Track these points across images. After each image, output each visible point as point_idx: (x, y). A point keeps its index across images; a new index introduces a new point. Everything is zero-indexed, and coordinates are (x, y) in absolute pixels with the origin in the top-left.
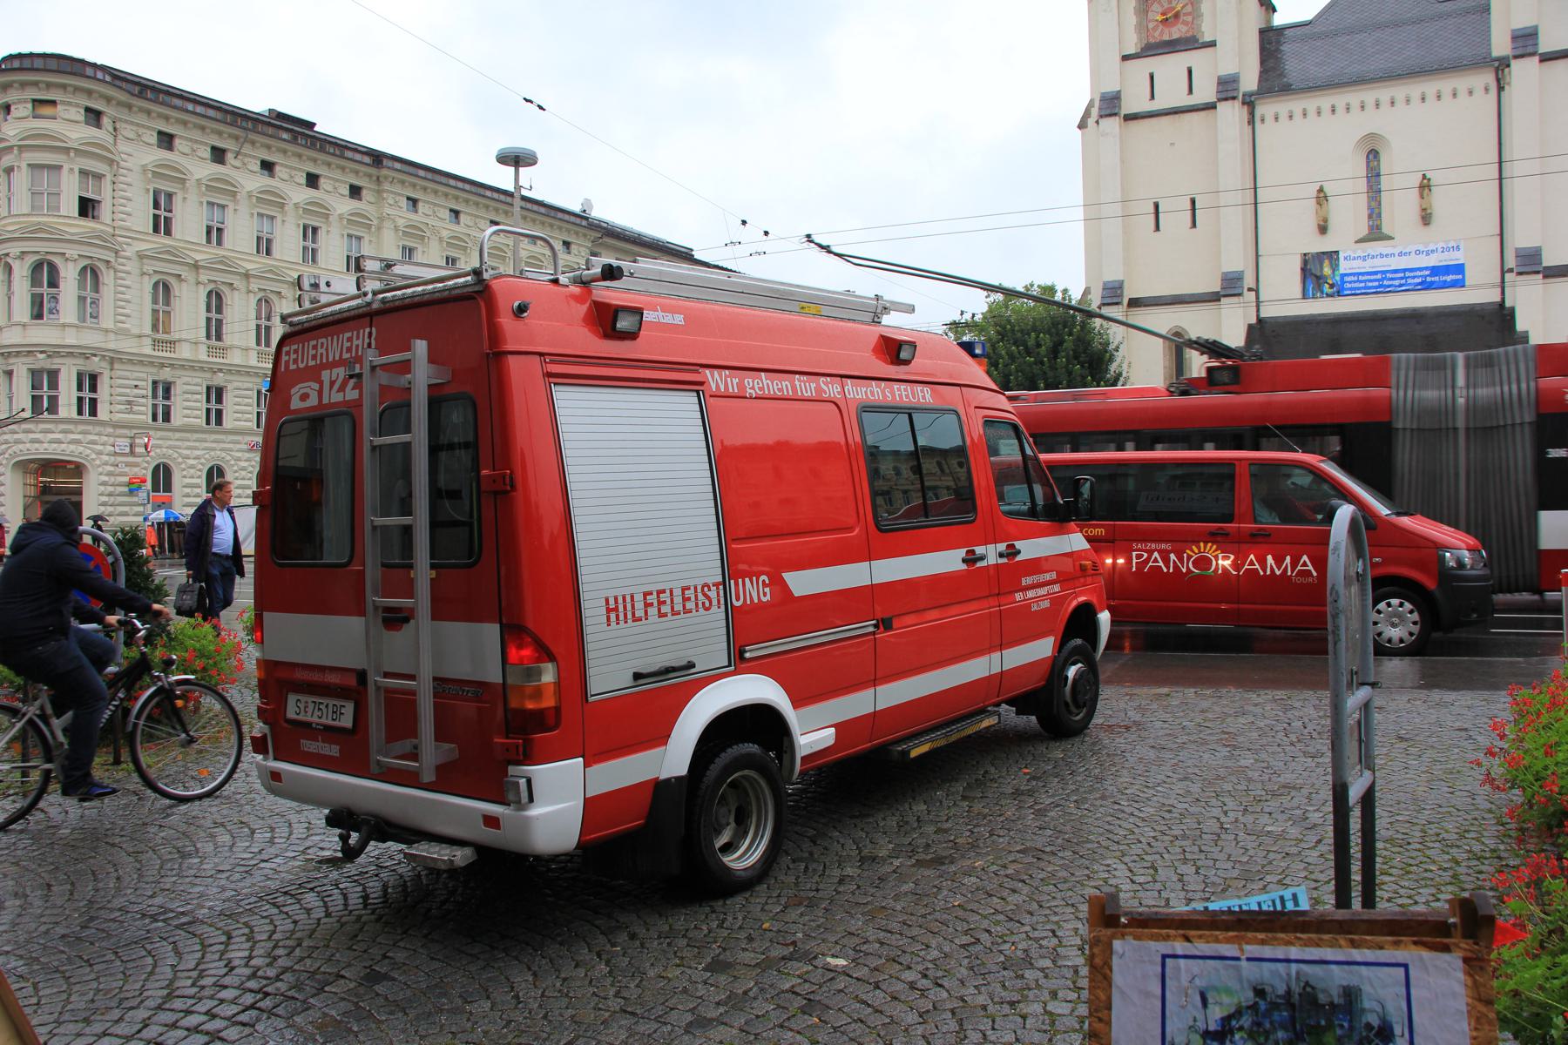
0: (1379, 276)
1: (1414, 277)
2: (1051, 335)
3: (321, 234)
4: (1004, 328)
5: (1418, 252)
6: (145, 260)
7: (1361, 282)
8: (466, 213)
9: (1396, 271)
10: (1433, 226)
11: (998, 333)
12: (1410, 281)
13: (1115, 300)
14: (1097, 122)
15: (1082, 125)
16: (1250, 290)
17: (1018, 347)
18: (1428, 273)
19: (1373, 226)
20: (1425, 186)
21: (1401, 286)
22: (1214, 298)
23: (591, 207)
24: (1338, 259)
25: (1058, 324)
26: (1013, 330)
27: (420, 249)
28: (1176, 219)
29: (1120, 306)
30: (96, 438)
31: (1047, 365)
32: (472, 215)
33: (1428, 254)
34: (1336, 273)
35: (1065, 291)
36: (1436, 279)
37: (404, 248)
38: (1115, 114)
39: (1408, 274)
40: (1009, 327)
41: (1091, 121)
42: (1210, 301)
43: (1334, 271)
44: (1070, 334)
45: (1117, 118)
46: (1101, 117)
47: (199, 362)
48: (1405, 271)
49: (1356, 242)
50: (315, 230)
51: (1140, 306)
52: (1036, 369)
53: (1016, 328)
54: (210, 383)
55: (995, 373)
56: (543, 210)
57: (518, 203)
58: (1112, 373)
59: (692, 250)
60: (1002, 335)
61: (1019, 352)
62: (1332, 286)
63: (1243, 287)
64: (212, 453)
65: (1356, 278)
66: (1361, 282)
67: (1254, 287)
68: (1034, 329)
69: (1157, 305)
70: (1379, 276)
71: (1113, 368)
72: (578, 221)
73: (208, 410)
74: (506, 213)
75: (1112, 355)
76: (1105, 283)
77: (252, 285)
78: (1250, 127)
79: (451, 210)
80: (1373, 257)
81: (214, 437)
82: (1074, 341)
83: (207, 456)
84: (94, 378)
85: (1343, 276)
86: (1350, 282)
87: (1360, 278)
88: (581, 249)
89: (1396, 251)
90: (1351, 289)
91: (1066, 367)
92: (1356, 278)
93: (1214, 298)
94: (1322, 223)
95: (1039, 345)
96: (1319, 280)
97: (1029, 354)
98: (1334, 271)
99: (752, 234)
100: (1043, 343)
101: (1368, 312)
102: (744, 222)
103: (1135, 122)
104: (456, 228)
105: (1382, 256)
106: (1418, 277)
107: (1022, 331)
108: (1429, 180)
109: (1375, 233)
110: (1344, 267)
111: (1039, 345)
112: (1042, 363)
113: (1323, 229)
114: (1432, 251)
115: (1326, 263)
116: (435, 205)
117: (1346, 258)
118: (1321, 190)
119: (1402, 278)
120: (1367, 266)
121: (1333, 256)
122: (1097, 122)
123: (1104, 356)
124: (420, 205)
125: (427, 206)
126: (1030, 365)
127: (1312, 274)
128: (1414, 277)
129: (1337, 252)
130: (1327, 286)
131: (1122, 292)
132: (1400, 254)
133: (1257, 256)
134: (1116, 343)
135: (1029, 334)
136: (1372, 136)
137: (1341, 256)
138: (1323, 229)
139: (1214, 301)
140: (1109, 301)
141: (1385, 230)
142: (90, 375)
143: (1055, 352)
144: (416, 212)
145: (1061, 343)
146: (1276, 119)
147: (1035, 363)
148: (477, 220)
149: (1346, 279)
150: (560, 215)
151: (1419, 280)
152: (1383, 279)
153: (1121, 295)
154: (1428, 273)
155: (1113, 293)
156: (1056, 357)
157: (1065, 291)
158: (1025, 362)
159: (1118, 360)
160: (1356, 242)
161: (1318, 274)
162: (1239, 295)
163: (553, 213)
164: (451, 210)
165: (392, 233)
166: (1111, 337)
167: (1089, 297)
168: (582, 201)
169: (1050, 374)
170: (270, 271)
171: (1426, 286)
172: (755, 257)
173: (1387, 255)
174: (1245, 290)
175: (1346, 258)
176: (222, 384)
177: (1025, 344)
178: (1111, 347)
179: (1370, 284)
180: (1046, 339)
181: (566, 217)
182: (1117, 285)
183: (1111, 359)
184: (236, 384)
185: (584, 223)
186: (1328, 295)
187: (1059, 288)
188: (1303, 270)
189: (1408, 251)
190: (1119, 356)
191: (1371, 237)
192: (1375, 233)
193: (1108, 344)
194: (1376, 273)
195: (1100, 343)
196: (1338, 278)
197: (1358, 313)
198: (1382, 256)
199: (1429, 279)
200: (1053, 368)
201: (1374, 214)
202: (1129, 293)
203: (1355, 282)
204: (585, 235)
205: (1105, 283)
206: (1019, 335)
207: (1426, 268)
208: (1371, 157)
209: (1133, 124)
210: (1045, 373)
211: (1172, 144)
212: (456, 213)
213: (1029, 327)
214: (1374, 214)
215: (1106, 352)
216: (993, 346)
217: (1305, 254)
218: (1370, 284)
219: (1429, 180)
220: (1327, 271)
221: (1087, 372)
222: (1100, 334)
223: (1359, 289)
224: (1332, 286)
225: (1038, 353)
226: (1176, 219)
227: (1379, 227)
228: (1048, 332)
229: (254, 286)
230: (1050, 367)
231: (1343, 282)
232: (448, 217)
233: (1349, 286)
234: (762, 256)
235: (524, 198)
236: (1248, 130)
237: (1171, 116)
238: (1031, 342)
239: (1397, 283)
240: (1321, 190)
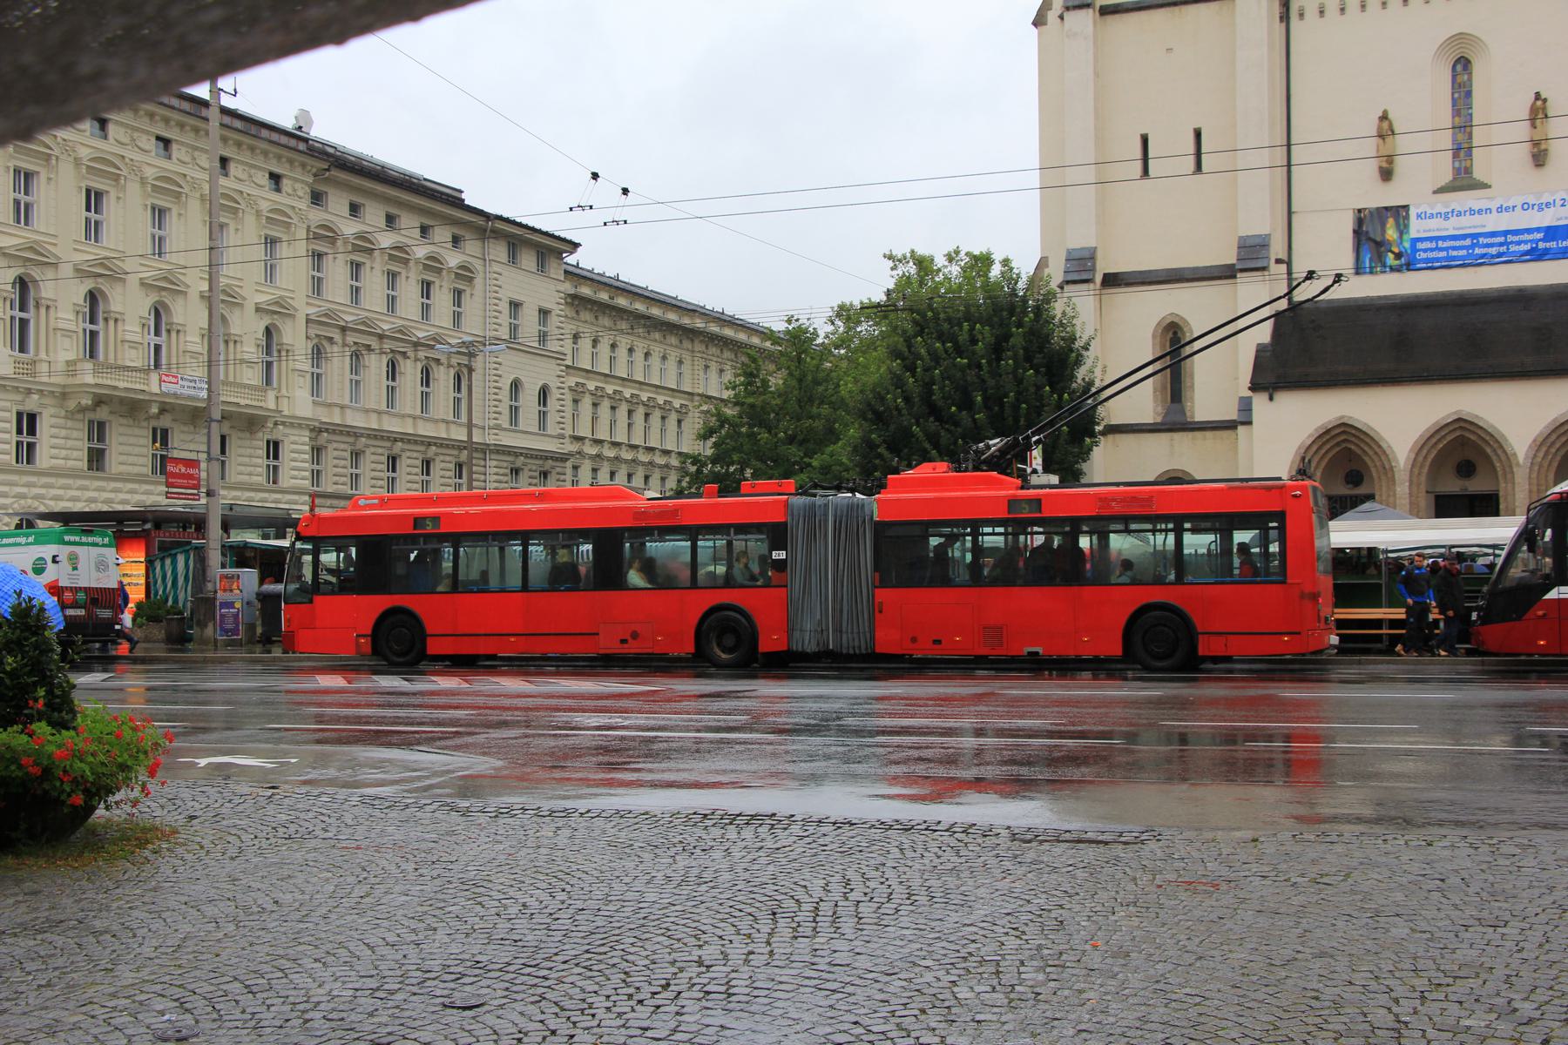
0: (1468, 242)
1: (1519, 243)
2: (992, 327)
3: (109, 203)
4: (924, 316)
5: (1526, 206)
6: (420, 348)
7: (1441, 250)
8: (182, 144)
9: (1493, 234)
10: (1549, 169)
11: (915, 322)
12: (1513, 248)
13: (1085, 276)
14: (1061, 17)
15: (1039, 21)
16: (1278, 261)
17: (943, 344)
18: (1540, 236)
19: (1459, 169)
20: (1539, 110)
21: (1500, 255)
22: (1227, 273)
23: (310, 122)
24: (1407, 217)
25: (1002, 310)
26: (936, 318)
27: (113, 194)
28: (1172, 147)
29: (1091, 286)
30: (25, 490)
31: (985, 368)
32: (187, 145)
33: (1540, 209)
34: (1405, 237)
35: (1006, 262)
36: (1553, 245)
37: (17, 171)
38: (1088, 6)
39: (1510, 238)
40: (930, 314)
41: (1052, 16)
42: (1220, 278)
43: (1401, 234)
44: (1020, 325)
45: (1091, 11)
46: (1068, 9)
47: (346, 426)
48: (1506, 233)
49: (1435, 192)
50: (99, 195)
51: (1119, 285)
52: (971, 376)
53: (942, 316)
54: (21, 408)
55: (911, 380)
56: (238, 124)
57: (213, 114)
58: (1079, 381)
59: (461, 192)
60: (921, 328)
61: (946, 351)
62: (1398, 256)
63: (1268, 258)
64: (22, 502)
65: (1433, 245)
66: (1441, 250)
67: (1286, 259)
68: (968, 317)
69: (1151, 283)
70: (1468, 242)
71: (1081, 373)
72: (293, 143)
73: (268, 466)
74: (196, 130)
75: (1080, 355)
76: (1069, 252)
77: (348, 338)
78: (1284, 24)
79: (159, 138)
80: (1459, 215)
81: (26, 479)
82: (1024, 335)
83: (16, 506)
84: (32, 418)
85: (1415, 241)
86: (1425, 251)
87: (1440, 244)
88: (298, 186)
89: (1494, 205)
90: (1427, 260)
91: (1014, 372)
92: (1433, 245)
93: (1227, 273)
94: (1385, 165)
95: (974, 341)
96: (1380, 246)
97: (960, 353)
98: (1401, 234)
99: (602, 191)
100: (980, 337)
101: (1451, 293)
102: (595, 176)
103: (1117, 16)
104: (100, 144)
105: (1472, 212)
106: (1526, 242)
107: (949, 320)
108: (1545, 101)
109: (1463, 180)
110: (1416, 228)
111: (974, 341)
112: (979, 366)
113: (1386, 174)
114: (1548, 205)
115: (1391, 221)
116: (196, 148)
117: (1419, 216)
118: (1384, 117)
119: (1501, 244)
120: (1451, 227)
121: (1399, 213)
122: (1061, 17)
123: (1068, 356)
124: (174, 147)
125: (184, 149)
126: (962, 369)
127: (1370, 239)
128: (1519, 243)
129: (1406, 207)
130: (1391, 256)
131: (1094, 265)
132: (1500, 209)
133: (1290, 213)
134: (1085, 338)
135: (960, 325)
136: (1460, 38)
137: (1413, 212)
138: (1386, 174)
139: (1226, 278)
140: (1075, 277)
141: (1478, 174)
142: (28, 414)
143: (997, 350)
144: (106, 138)
145: (1007, 337)
146: (1322, 13)
147: (969, 366)
148: (136, 135)
149: (1420, 246)
150: (265, 133)
151: (1527, 247)
152: (1473, 246)
153: (1093, 269)
154: (1540, 236)
155: (1081, 268)
156: (999, 359)
157: (1006, 262)
158: (955, 365)
159: (1088, 363)
160: (1435, 192)
161: (1378, 239)
162: (1264, 269)
163: (254, 130)
164: (159, 138)
165: (253, 218)
166: (1078, 328)
167: (1047, 271)
168: (295, 112)
169: (991, 382)
170: (364, 323)
171: (1537, 255)
172: (612, 228)
173: (1480, 212)
174: (1273, 261)
175: (1419, 216)
176: (281, 438)
177: (953, 339)
178: (1078, 344)
179: (1455, 253)
180: (986, 334)
181: (275, 137)
182: (1087, 254)
183: (1078, 362)
184: (293, 438)
185: (302, 146)
186: (1393, 269)
187: (998, 257)
188: (1358, 233)
189: (1510, 204)
190: (1090, 356)
191: (1458, 183)
192: (1463, 180)
193: (1073, 339)
194: (1464, 237)
195: (1063, 339)
196: (1407, 245)
197: (1437, 294)
198: (1472, 212)
199: (1541, 245)
200: (995, 374)
201: (1462, 150)
202: (1104, 266)
203: (1432, 250)
204: (303, 166)
205: (1069, 252)
206: (946, 326)
207: (1538, 230)
208: (1459, 68)
209: (1112, 20)
210: (983, 381)
211: (1169, 50)
212: (166, 142)
213: (960, 315)
214: (1462, 150)
215: (1071, 350)
216: (908, 342)
217: (1359, 211)
218: (1455, 253)
219: (1545, 101)
220: (1391, 233)
221: (1044, 380)
222: (1061, 324)
223: (1438, 260)
224: (1398, 256)
225: (974, 353)
226: (1172, 147)
227: (1468, 171)
228: (988, 322)
229: (350, 339)
230: (989, 372)
231: (1414, 250)
232: (154, 148)
233: (1423, 255)
234: (622, 226)
235: (225, 111)
236: (1279, 28)
237: (1168, 9)
238: (963, 337)
239: (1493, 251)
240: (1384, 117)
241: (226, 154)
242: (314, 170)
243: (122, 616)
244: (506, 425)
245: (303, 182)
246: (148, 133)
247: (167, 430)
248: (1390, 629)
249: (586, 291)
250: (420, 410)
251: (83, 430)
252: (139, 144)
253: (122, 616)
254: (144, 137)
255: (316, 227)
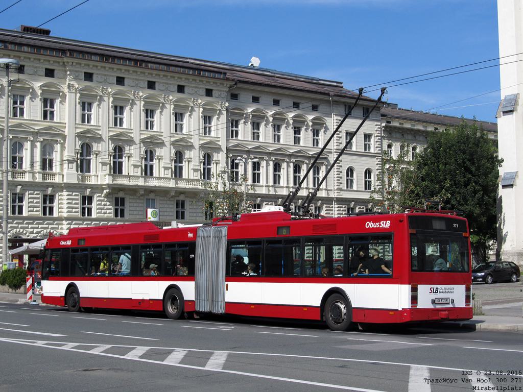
8: (189, 86)
142: (121, 198)
241: (182, 84)
242: (228, 86)
243: (461, 326)
244: (345, 188)
245: (223, 91)
246: (143, 80)
247: (124, 199)
248: (410, 366)
249: (395, 124)
250: (346, 187)
251: (174, 204)
252: (109, 81)
253: (461, 326)
254: (142, 82)
255: (232, 109)
